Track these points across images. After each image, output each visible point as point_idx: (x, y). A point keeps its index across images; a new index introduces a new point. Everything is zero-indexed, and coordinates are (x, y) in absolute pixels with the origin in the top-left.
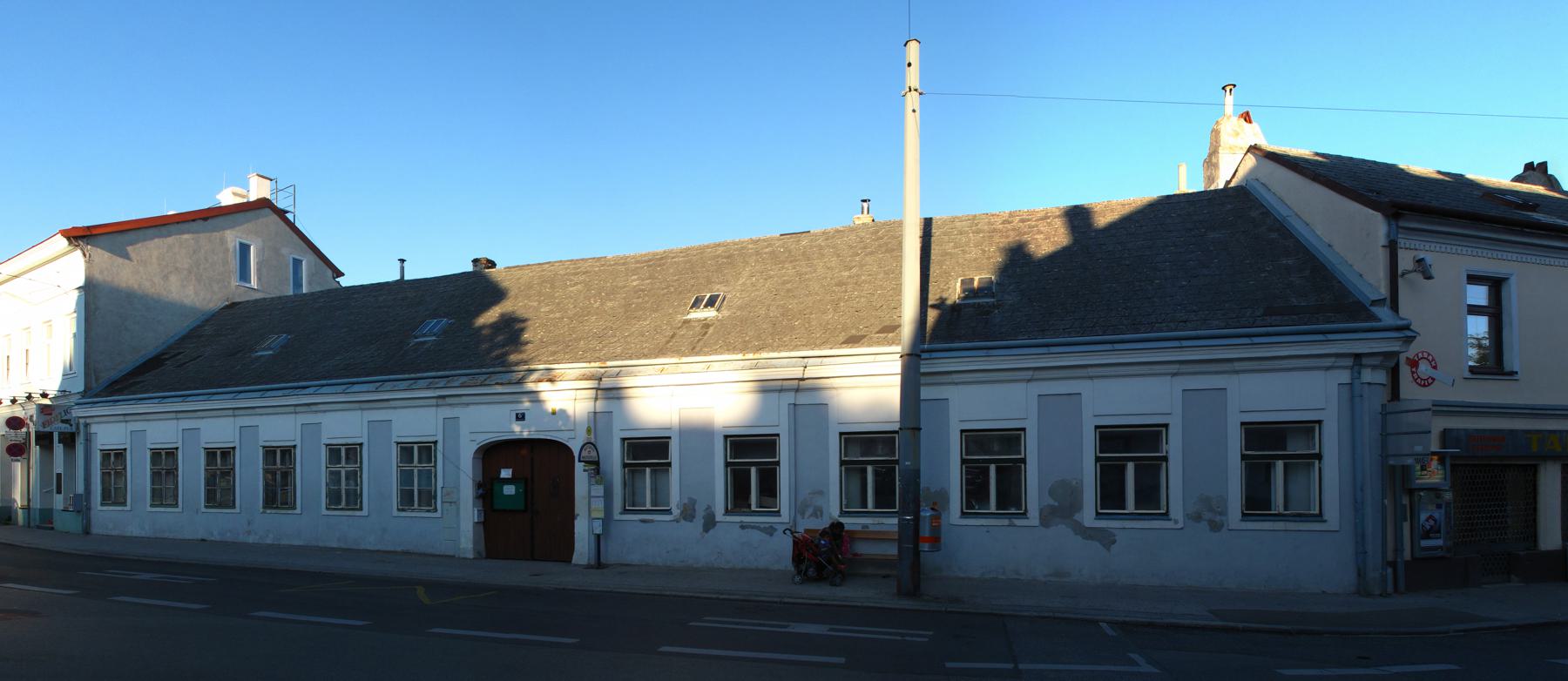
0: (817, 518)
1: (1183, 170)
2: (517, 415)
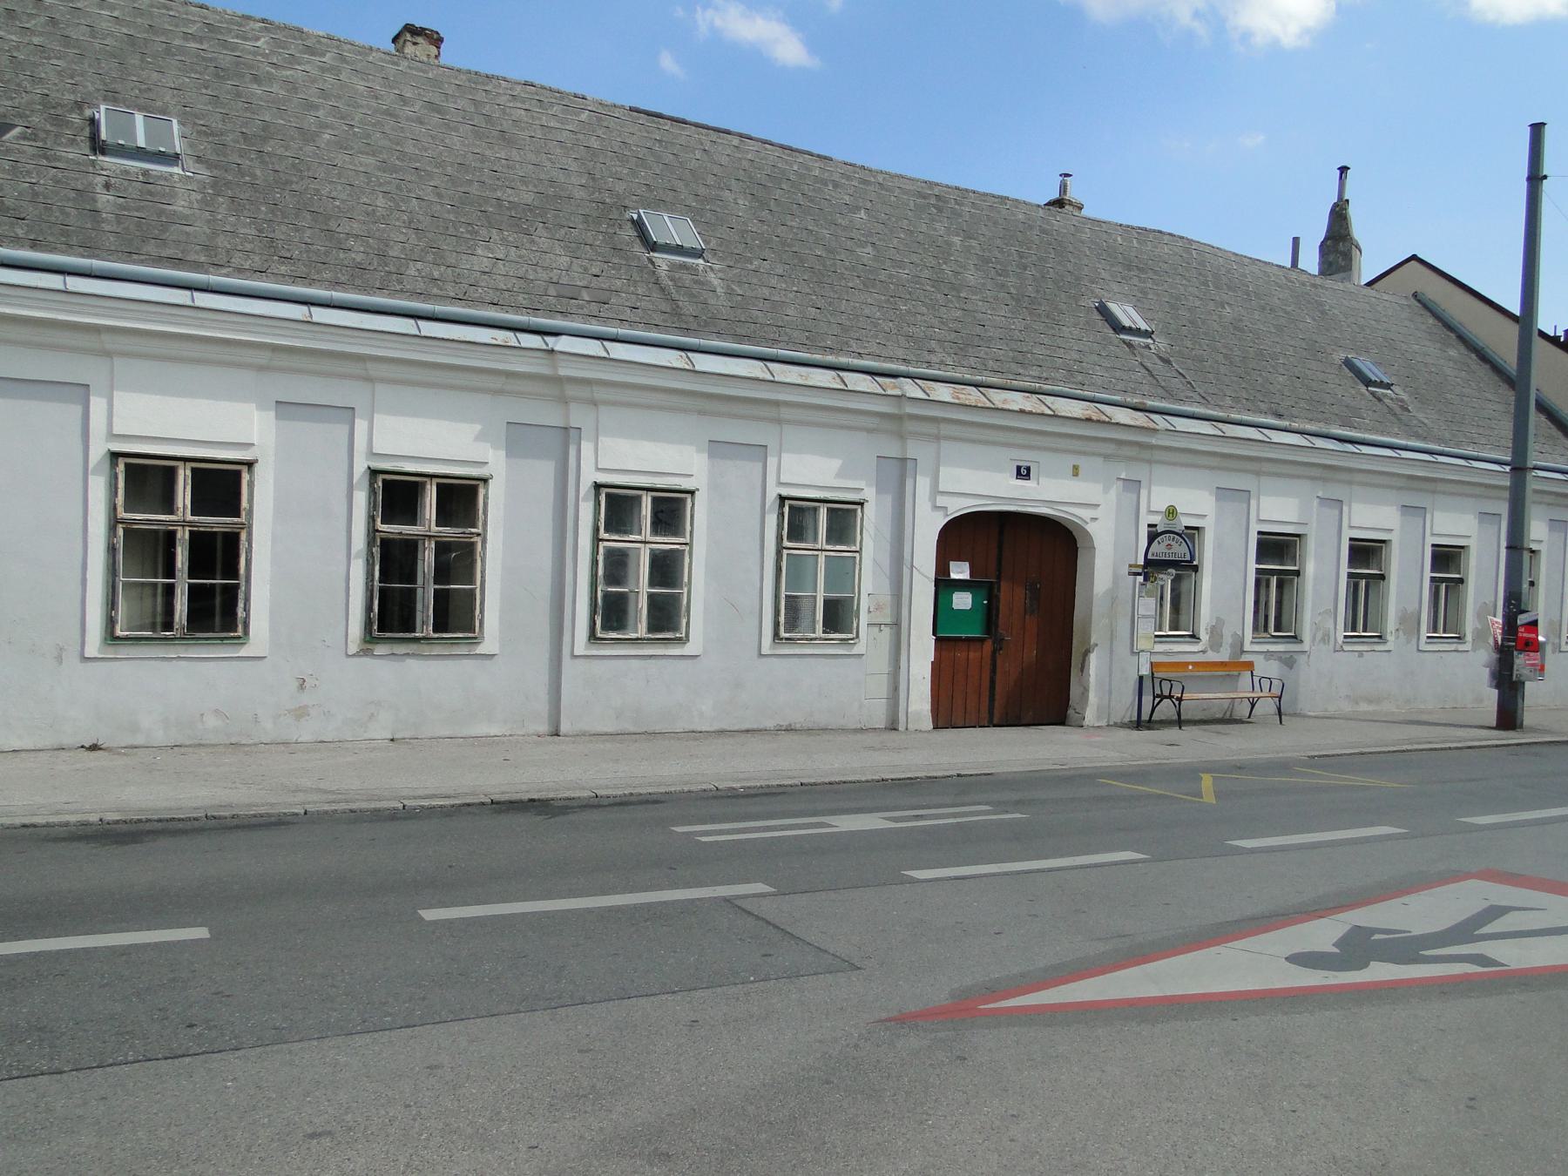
0: (1325, 643)
1: (789, 49)
2: (1019, 468)
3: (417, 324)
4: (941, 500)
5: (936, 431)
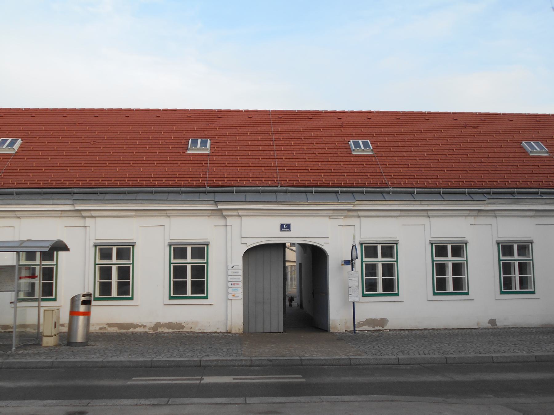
3: (383, 195)
4: (244, 241)
5: (357, 215)
